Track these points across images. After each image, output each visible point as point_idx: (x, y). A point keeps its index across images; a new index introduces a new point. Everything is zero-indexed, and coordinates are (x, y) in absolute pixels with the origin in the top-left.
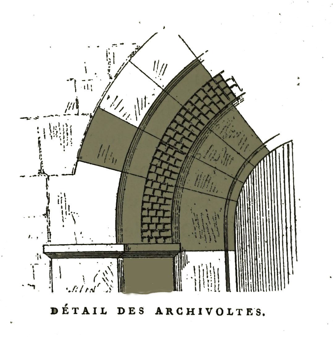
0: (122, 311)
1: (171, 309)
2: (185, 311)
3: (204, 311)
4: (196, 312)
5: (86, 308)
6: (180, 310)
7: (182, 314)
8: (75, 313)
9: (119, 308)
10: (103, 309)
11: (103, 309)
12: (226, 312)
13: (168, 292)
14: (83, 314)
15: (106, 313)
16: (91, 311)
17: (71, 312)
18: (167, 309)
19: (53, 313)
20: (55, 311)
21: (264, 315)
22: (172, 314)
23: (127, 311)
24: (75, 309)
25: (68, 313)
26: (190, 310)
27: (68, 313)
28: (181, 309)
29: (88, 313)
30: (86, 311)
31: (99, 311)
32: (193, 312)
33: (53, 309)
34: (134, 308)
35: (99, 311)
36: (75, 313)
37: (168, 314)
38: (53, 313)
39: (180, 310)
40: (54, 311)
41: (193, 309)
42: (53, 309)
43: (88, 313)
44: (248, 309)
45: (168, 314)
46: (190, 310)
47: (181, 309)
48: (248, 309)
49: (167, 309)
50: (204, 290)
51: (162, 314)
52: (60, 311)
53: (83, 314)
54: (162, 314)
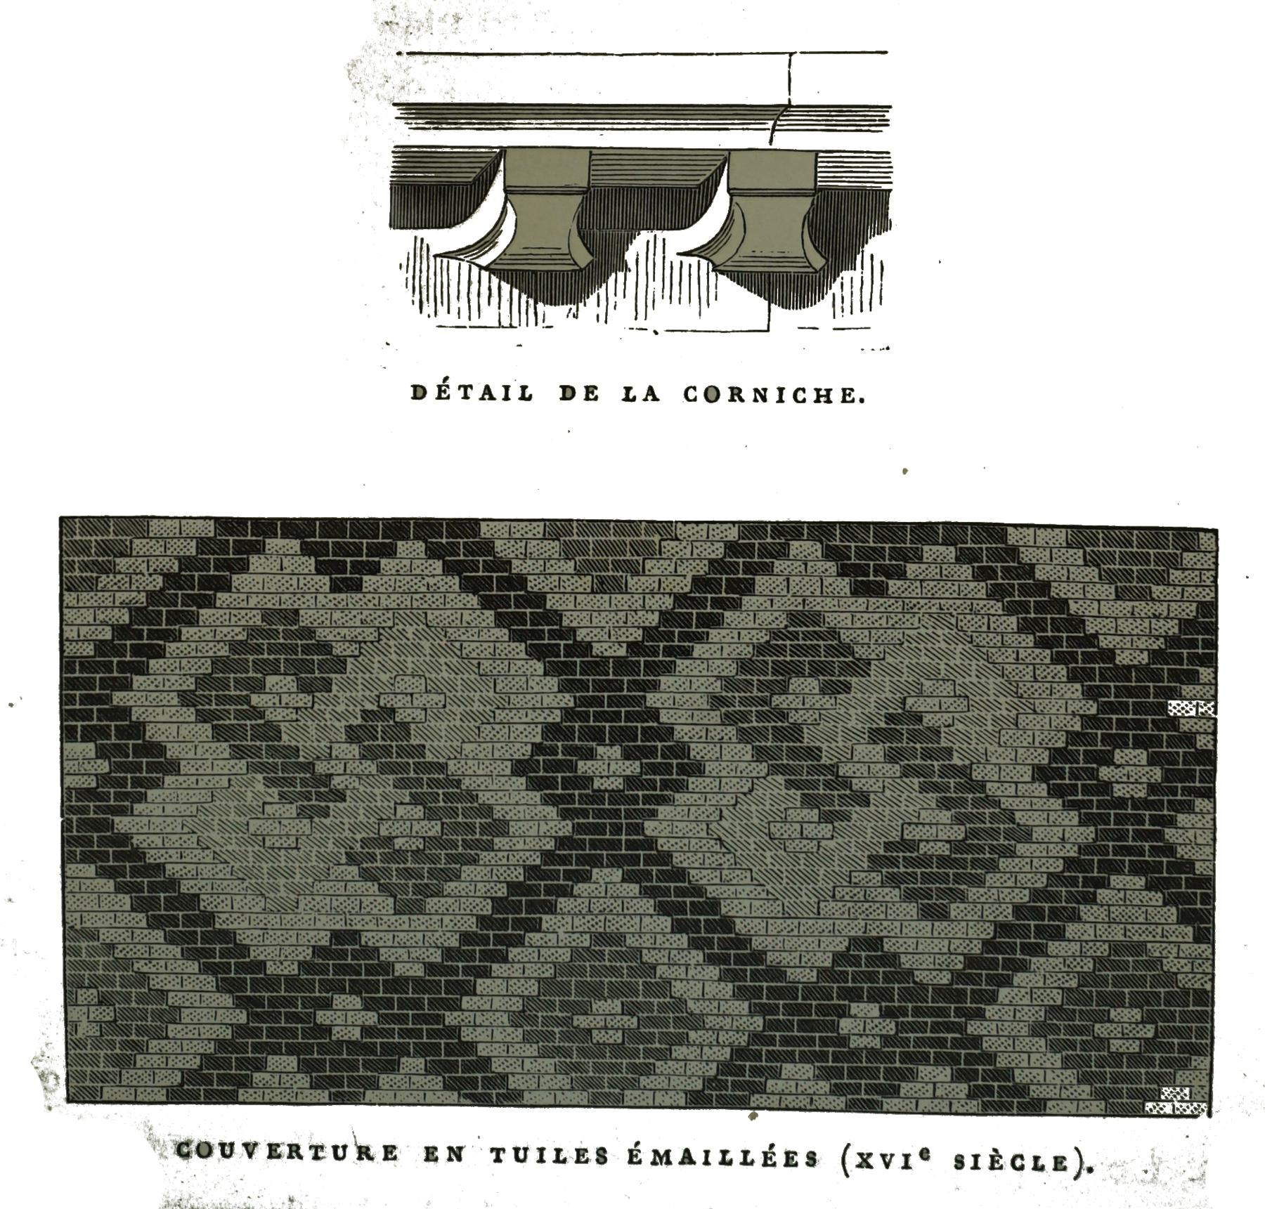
0: (420, 393)
1: (740, 390)
2: (811, 396)
3: (498, 392)
4: (772, 395)
5: (651, 389)
6: (800, 393)
7: (804, 401)
8: (466, 397)
9: (415, 387)
10: (524, 388)
11: (524, 388)
12: (1029, 1163)
13: (483, 199)
14: (482, 399)
15: (530, 398)
16: (498, 392)
17: (456, 394)
18: (732, 389)
19: (564, 398)
20: (420, 393)
21: (862, 401)
22: (742, 400)
23: (581, 393)
24: (466, 387)
25: (448, 398)
26: (823, 393)
27: (448, 398)
28: (695, 388)
29: (492, 398)
30: (488, 393)
31: (515, 393)
32: (828, 396)
33: (564, 388)
34: (852, 390)
35: (515, 393)
36: (466, 397)
37: (732, 400)
38: (564, 398)
39: (800, 393)
40: (419, 392)
41: (828, 391)
42: (564, 388)
43: (492, 398)
44: (386, 1147)
45: (732, 400)
46: (823, 393)
47: (804, 390)
48: (386, 1147)
49: (732, 389)
50: (888, 116)
51: (694, 1163)
52: (432, 392)
53: (482, 399)
54: (694, 1163)
